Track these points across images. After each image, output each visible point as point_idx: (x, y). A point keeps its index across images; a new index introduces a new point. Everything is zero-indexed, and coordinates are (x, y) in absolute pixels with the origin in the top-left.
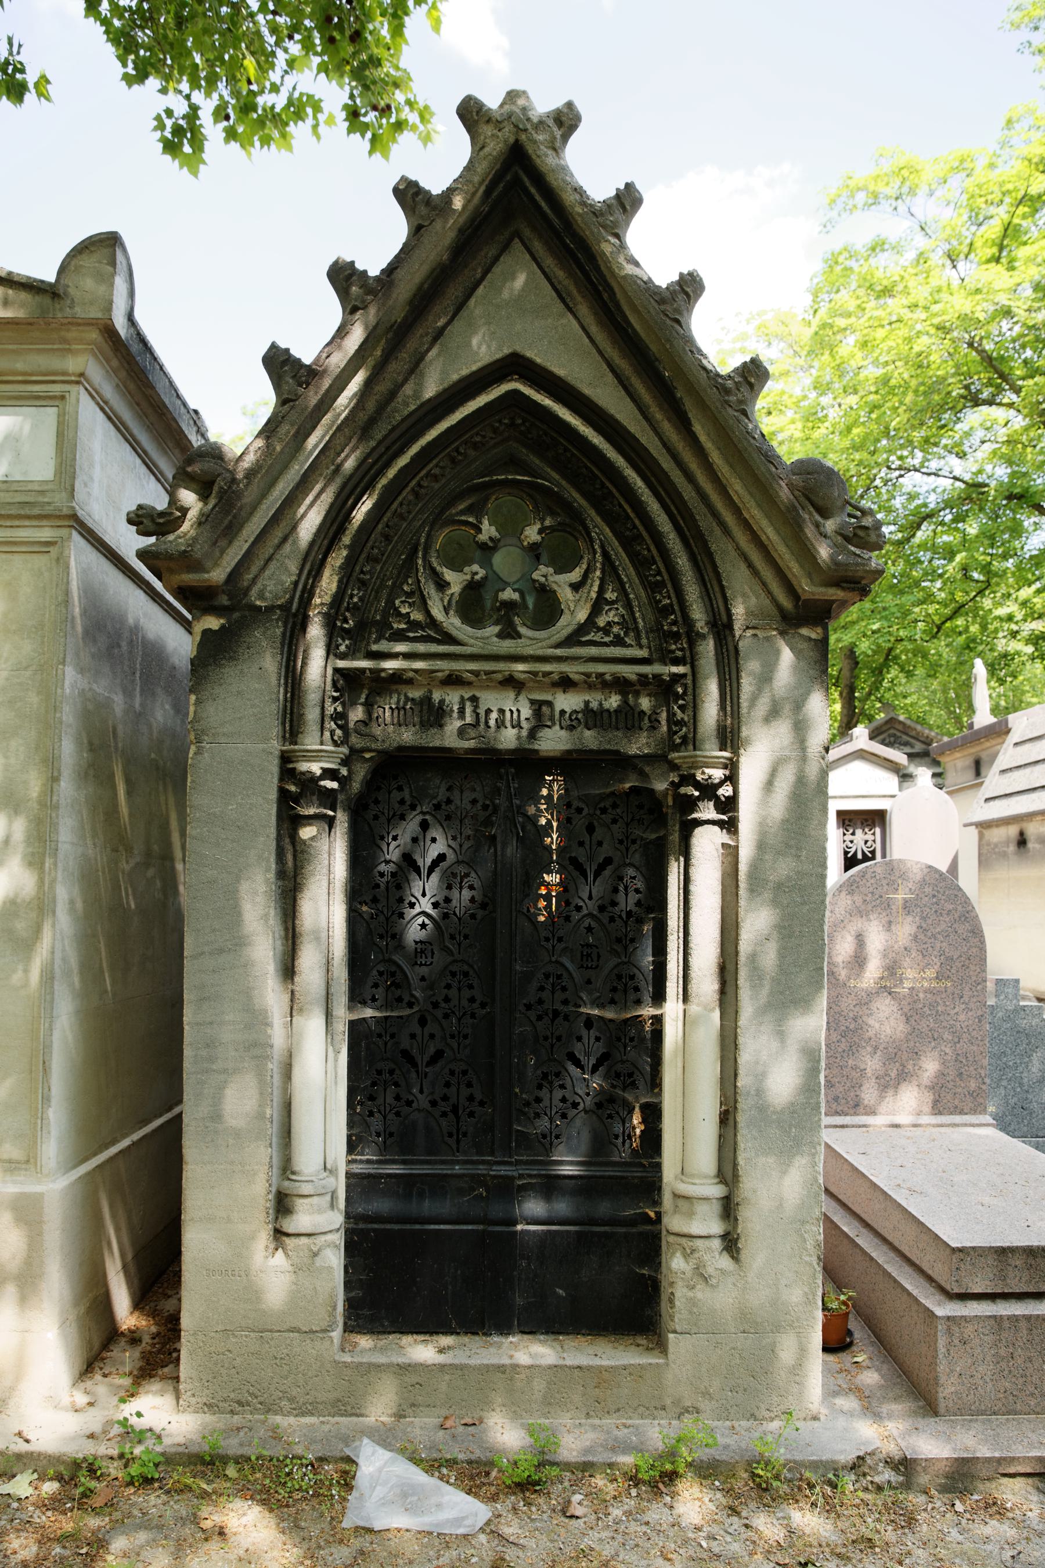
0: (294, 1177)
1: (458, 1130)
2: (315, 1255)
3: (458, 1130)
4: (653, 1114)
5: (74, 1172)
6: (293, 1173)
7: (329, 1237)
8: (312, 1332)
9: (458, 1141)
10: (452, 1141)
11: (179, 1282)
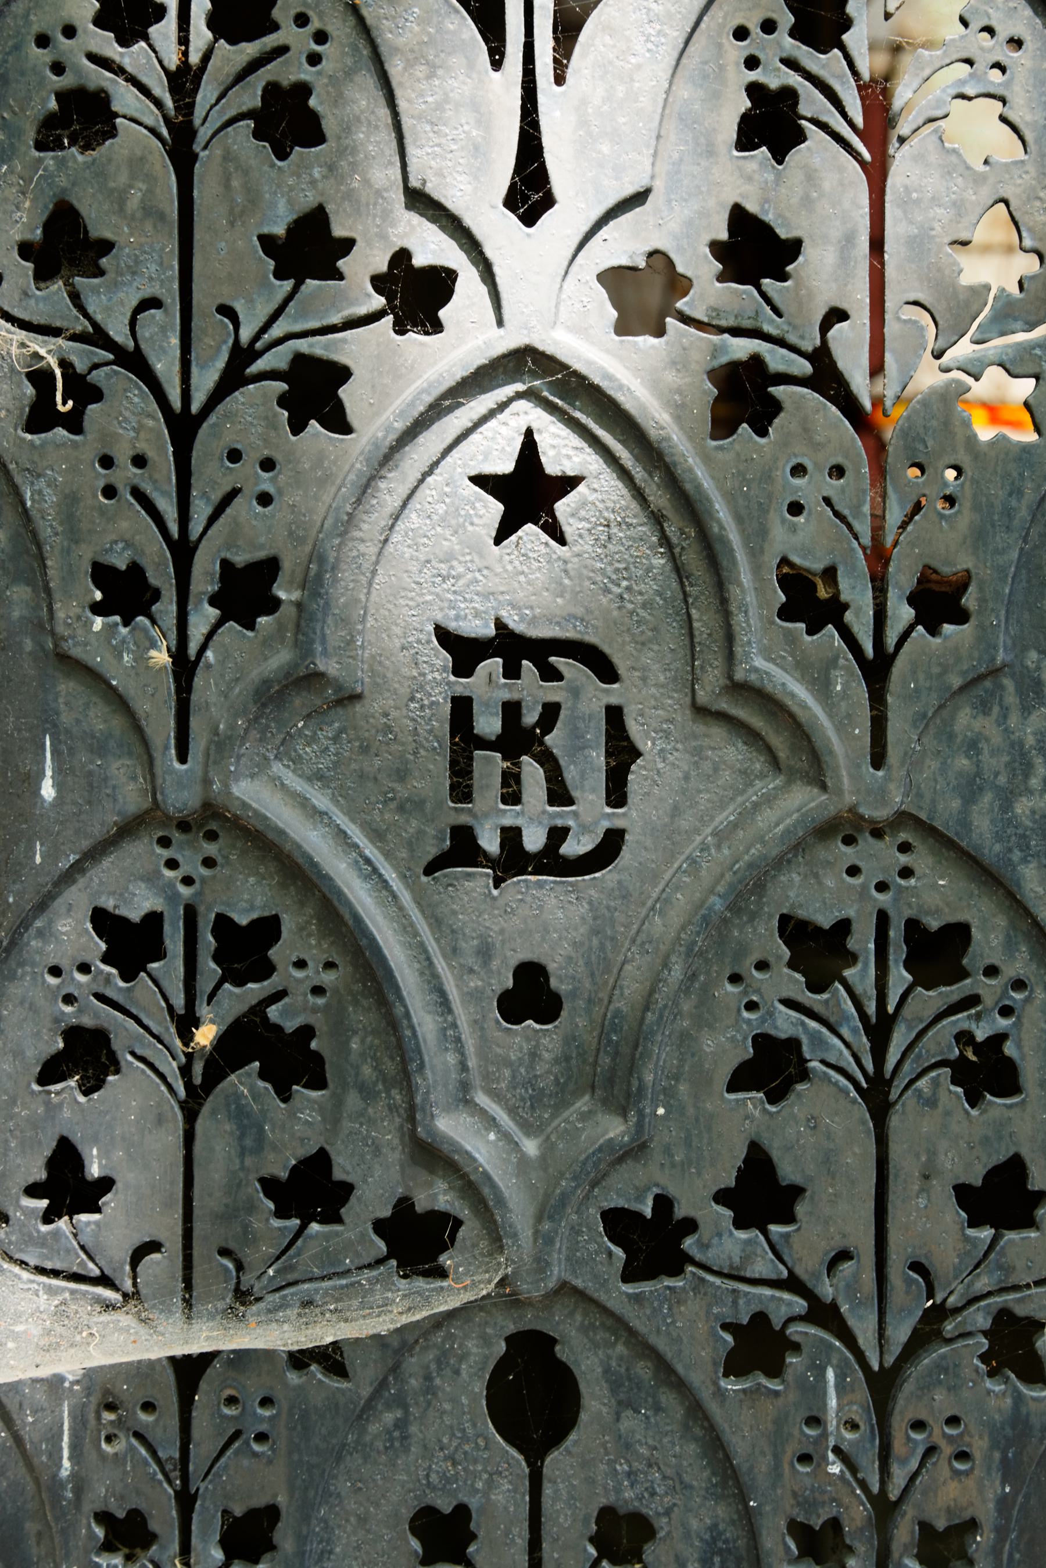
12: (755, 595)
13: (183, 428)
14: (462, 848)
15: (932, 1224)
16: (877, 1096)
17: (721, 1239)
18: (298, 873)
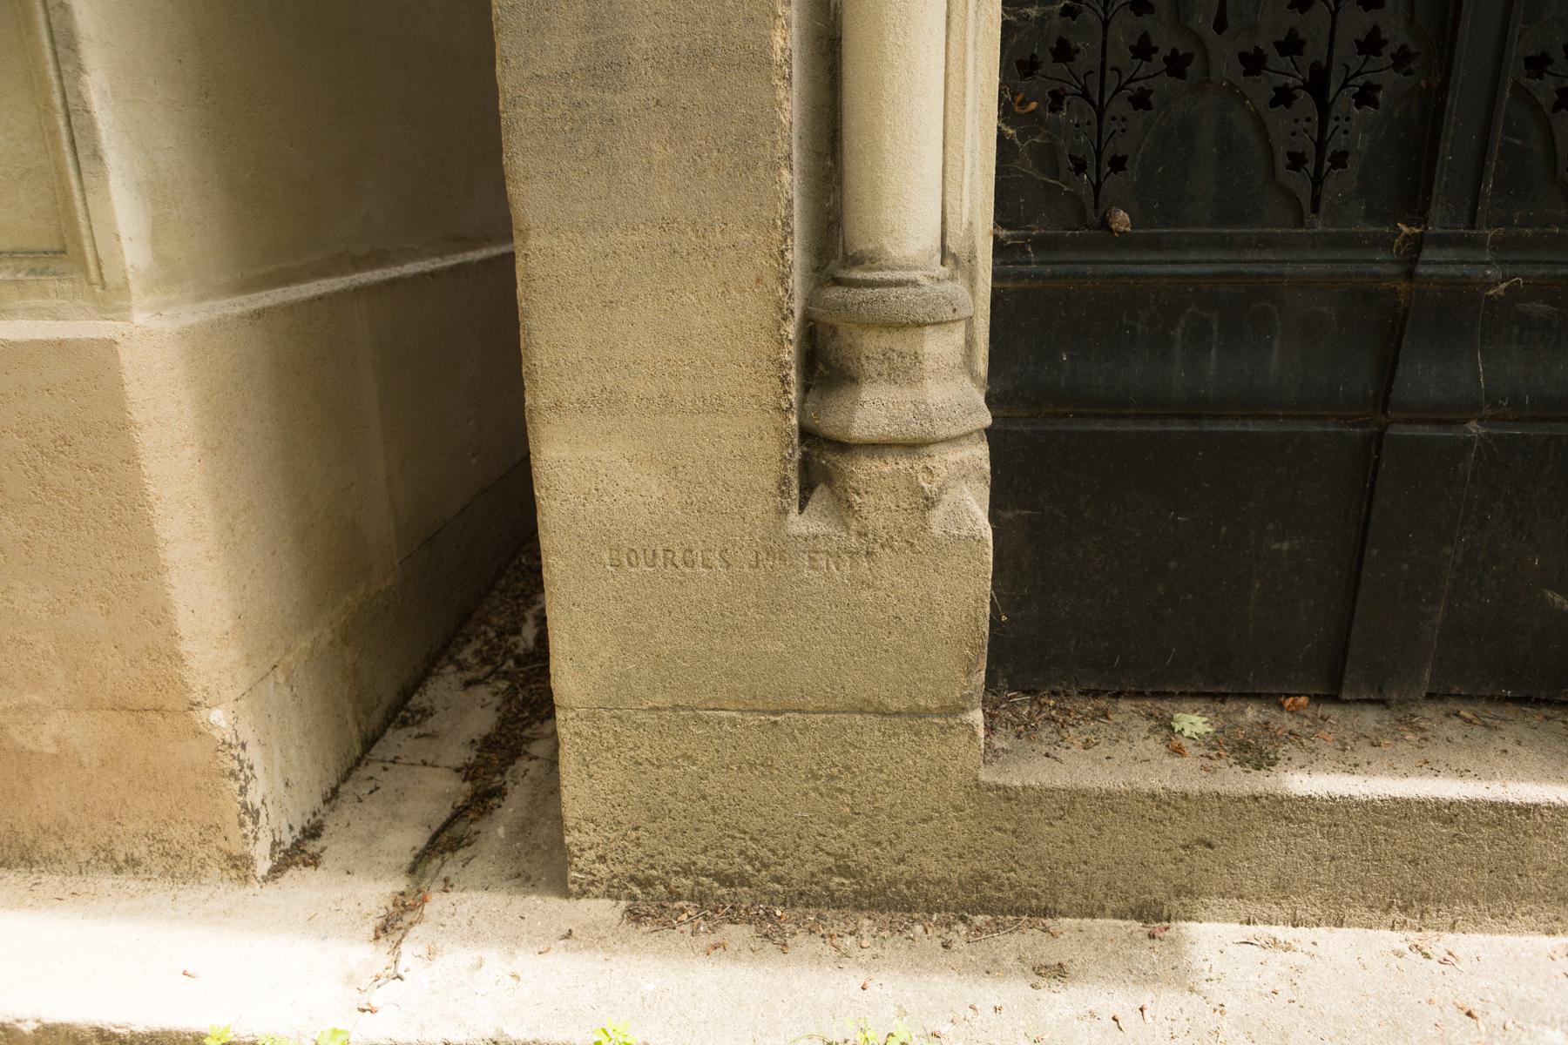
0: (858, 274)
1: (1321, 145)
2: (930, 503)
3: (1321, 145)
4: (542, 621)
5: (242, 298)
6: (857, 261)
7: (953, 455)
8: (916, 713)
9: (1317, 180)
10: (1299, 183)
11: (539, 586)
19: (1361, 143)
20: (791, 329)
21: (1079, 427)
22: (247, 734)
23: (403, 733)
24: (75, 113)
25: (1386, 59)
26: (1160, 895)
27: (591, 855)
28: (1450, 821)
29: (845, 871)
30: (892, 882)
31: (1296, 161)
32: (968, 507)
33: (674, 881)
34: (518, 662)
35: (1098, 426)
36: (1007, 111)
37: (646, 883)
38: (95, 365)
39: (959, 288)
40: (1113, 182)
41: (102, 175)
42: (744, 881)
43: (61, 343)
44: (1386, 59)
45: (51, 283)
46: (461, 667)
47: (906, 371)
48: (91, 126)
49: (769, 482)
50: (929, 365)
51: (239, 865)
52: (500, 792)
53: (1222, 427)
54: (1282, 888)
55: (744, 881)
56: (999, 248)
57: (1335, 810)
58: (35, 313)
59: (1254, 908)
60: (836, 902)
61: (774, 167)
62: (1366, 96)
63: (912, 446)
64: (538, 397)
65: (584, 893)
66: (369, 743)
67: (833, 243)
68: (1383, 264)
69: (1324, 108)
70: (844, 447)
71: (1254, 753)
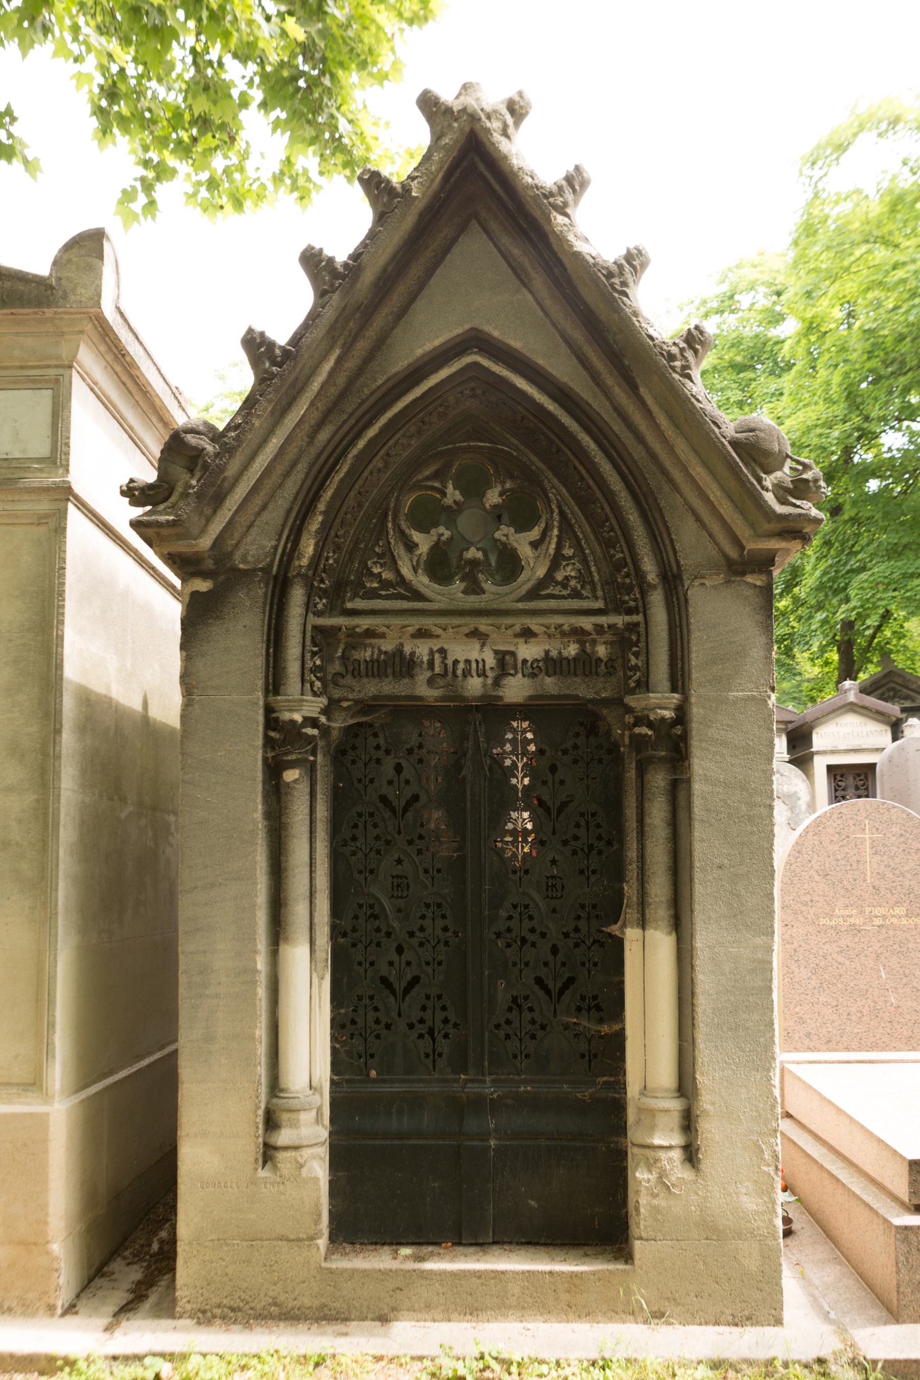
1: (434, 1051)
2: (302, 1166)
3: (434, 1051)
6: (282, 1091)
8: (299, 1240)
9: (434, 1061)
12: (421, 871)
13: (366, 856)
14: (393, 896)
15: (439, 932)
16: (433, 920)
17: (418, 934)
18: (377, 899)
19: (446, 1050)
20: (261, 1112)
21: (363, 1142)
22: (62, 1256)
23: (102, 1280)
24: (50, 1045)
25: (450, 1025)
26: (386, 1311)
27: (185, 1300)
28: (479, 1277)
29: (276, 1304)
30: (293, 1309)
31: (427, 1055)
32: (318, 1169)
33: (214, 1311)
34: (151, 1256)
35: (369, 1142)
36: (334, 1039)
37: (204, 1312)
38: (41, 1122)
39: (317, 1097)
40: (370, 1062)
41: (54, 1062)
42: (239, 1309)
43: (32, 1114)
44: (450, 1025)
45: (29, 1094)
46: (124, 1258)
47: (295, 1125)
48: (54, 1048)
49: (252, 1160)
50: (302, 1122)
51: (51, 1308)
52: (147, 1296)
53: (411, 1142)
54: (428, 1307)
55: (239, 1309)
56: (333, 1082)
57: (441, 1274)
58: (22, 1103)
59: (420, 1316)
60: (272, 1317)
61: (255, 1066)
62: (446, 1036)
63: (296, 1148)
64: (181, 1133)
65: (180, 1317)
66: (90, 1281)
67: (275, 1085)
68: (456, 1087)
69: (434, 1040)
70: (276, 1148)
71: (421, 1259)
